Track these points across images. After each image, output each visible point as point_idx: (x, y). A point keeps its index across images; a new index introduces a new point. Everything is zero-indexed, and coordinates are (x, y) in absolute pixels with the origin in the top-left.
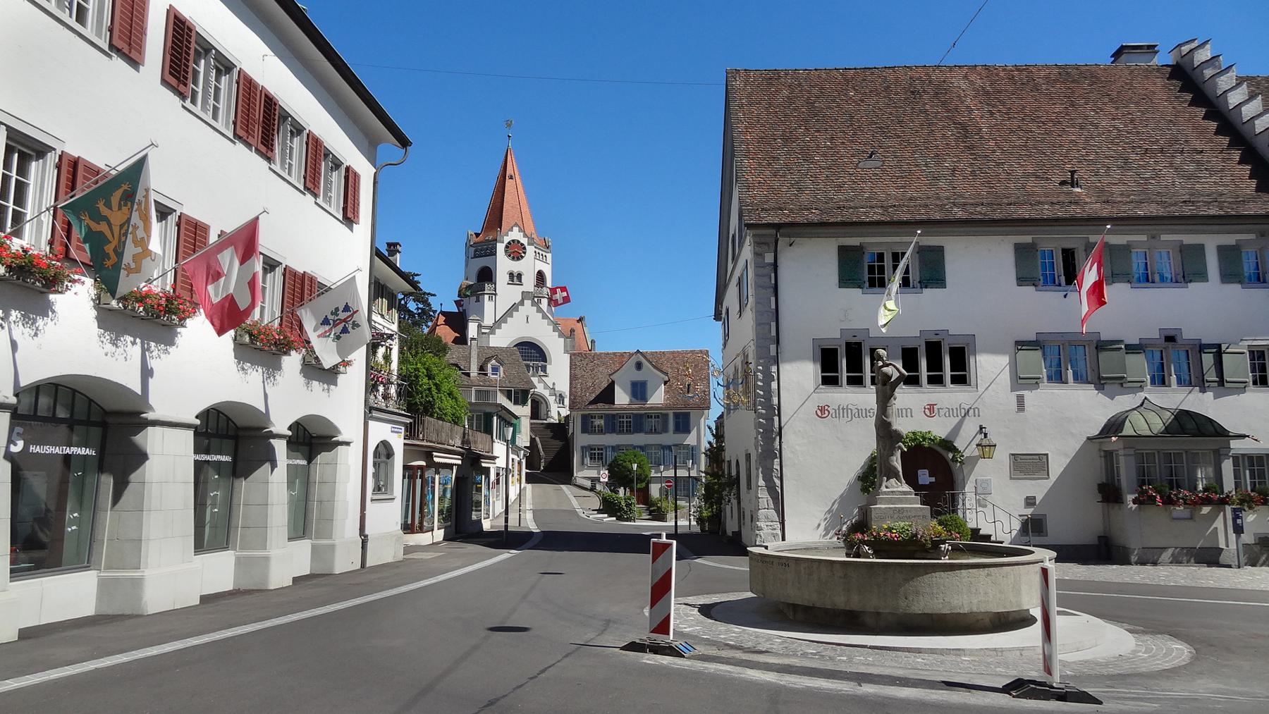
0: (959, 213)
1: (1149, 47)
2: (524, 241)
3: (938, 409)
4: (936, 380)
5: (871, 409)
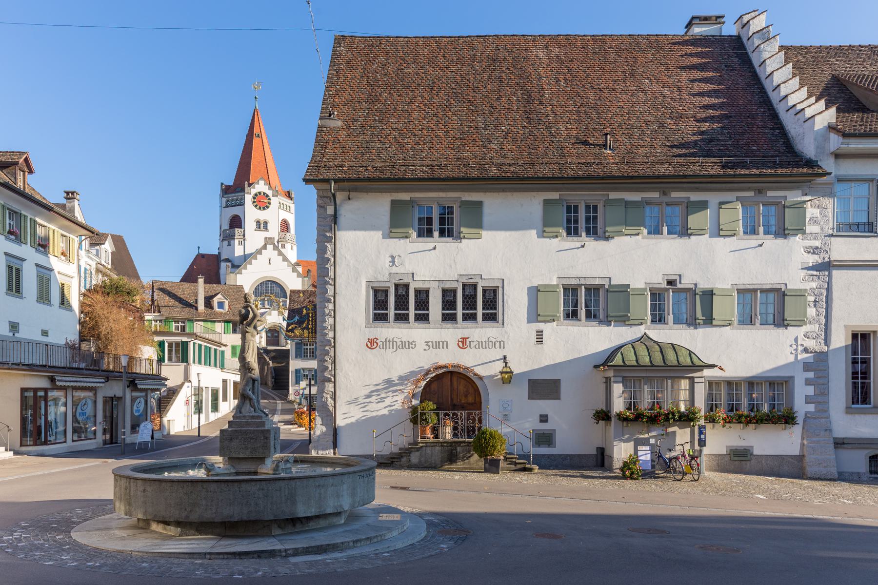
0: (494, 171)
1: (718, 17)
2: (270, 193)
3: (470, 342)
4: (470, 317)
5: (414, 342)
